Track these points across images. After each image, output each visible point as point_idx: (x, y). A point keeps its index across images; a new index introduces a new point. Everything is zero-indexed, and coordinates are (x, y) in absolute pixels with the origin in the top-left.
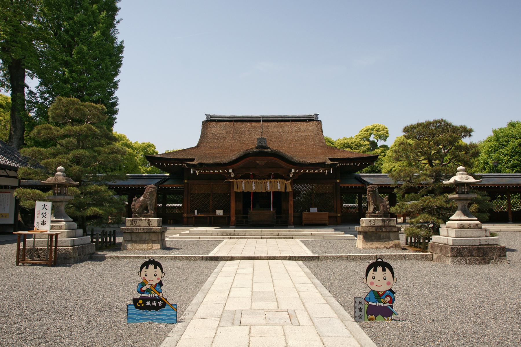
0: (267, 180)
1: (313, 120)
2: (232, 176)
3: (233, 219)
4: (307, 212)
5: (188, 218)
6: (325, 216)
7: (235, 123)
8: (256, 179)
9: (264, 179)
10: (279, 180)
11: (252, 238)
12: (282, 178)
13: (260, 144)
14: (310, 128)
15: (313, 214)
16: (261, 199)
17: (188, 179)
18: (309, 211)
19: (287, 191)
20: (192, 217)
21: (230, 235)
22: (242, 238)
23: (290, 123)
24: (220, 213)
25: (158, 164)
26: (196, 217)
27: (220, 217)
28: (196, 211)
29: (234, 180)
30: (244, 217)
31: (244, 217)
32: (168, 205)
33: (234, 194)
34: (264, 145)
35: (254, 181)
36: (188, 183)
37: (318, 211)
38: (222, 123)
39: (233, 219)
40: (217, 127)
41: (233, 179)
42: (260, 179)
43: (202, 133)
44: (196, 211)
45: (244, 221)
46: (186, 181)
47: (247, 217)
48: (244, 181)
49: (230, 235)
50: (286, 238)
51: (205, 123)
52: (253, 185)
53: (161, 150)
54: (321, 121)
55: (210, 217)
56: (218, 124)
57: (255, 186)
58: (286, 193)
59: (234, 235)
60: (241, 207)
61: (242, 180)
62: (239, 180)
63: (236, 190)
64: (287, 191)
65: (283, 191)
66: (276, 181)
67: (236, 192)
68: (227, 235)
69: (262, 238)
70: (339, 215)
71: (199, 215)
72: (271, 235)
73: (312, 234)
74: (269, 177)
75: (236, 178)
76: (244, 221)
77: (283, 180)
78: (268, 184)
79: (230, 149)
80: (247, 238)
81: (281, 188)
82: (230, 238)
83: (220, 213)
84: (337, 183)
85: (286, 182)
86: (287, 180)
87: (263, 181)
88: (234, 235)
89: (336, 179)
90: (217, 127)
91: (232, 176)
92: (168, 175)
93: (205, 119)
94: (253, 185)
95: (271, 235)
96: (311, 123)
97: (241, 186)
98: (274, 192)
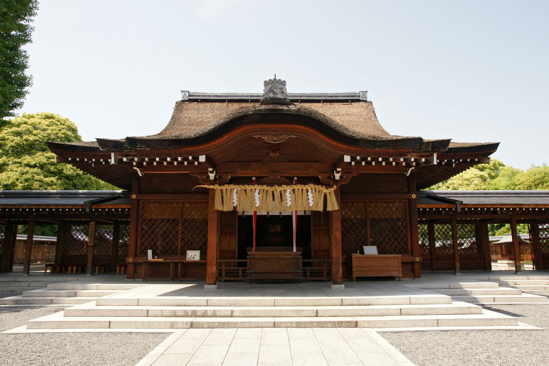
0: (285, 187)
1: (358, 101)
2: (212, 176)
3: (212, 269)
4: (358, 255)
5: (136, 265)
6: (394, 262)
7: (230, 104)
8: (262, 184)
9: (280, 185)
10: (310, 187)
11: (250, 326)
12: (317, 181)
13: (271, 95)
14: (355, 111)
15: (371, 257)
16: (270, 230)
17: (139, 192)
18: (362, 252)
19: (329, 209)
20: (141, 264)
21: (194, 314)
22: (222, 325)
23: (320, 104)
24: (193, 255)
25: (82, 160)
26: (150, 264)
27: (194, 264)
28: (150, 252)
29: (216, 187)
30: (240, 264)
31: (240, 264)
32: (36, 238)
33: (215, 216)
34: (280, 96)
35: (258, 188)
36: (138, 200)
37: (380, 253)
38: (208, 105)
39: (212, 269)
40: (198, 110)
41: (214, 182)
42: (271, 184)
43: (173, 118)
44: (150, 252)
45: (240, 272)
46: (134, 196)
47: (244, 264)
48: (236, 188)
49: (194, 314)
50: (340, 324)
51: (180, 105)
52: (257, 196)
53: (88, 136)
54: (371, 102)
55: (176, 264)
56: (202, 105)
57: (261, 200)
58: (326, 214)
59: (205, 315)
60: (233, 244)
61: (232, 186)
62: (226, 186)
63: (218, 206)
64: (329, 209)
65: (321, 209)
66: (305, 187)
67: (218, 211)
68: (186, 315)
69: (275, 325)
70: (418, 259)
71: (156, 260)
72: (299, 314)
73: (401, 313)
74: (289, 181)
75: (219, 181)
76: (240, 272)
77: (319, 187)
78: (287, 194)
79: (210, 118)
80: (235, 325)
81: (316, 203)
82: (192, 325)
83: (193, 255)
84: (410, 200)
85: (325, 191)
86: (328, 186)
87: (278, 189)
88: (205, 315)
89: (409, 192)
90: (198, 110)
91: (212, 176)
92: (120, 191)
93: (181, 99)
94: (257, 196)
95: (299, 314)
96: (356, 104)
97: (231, 198)
98: (299, 218)
